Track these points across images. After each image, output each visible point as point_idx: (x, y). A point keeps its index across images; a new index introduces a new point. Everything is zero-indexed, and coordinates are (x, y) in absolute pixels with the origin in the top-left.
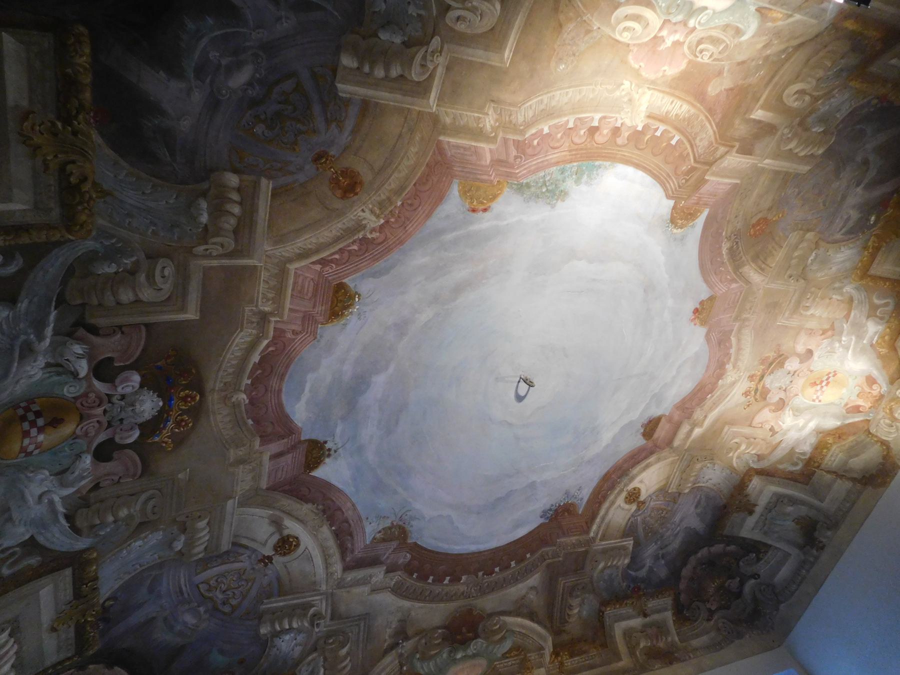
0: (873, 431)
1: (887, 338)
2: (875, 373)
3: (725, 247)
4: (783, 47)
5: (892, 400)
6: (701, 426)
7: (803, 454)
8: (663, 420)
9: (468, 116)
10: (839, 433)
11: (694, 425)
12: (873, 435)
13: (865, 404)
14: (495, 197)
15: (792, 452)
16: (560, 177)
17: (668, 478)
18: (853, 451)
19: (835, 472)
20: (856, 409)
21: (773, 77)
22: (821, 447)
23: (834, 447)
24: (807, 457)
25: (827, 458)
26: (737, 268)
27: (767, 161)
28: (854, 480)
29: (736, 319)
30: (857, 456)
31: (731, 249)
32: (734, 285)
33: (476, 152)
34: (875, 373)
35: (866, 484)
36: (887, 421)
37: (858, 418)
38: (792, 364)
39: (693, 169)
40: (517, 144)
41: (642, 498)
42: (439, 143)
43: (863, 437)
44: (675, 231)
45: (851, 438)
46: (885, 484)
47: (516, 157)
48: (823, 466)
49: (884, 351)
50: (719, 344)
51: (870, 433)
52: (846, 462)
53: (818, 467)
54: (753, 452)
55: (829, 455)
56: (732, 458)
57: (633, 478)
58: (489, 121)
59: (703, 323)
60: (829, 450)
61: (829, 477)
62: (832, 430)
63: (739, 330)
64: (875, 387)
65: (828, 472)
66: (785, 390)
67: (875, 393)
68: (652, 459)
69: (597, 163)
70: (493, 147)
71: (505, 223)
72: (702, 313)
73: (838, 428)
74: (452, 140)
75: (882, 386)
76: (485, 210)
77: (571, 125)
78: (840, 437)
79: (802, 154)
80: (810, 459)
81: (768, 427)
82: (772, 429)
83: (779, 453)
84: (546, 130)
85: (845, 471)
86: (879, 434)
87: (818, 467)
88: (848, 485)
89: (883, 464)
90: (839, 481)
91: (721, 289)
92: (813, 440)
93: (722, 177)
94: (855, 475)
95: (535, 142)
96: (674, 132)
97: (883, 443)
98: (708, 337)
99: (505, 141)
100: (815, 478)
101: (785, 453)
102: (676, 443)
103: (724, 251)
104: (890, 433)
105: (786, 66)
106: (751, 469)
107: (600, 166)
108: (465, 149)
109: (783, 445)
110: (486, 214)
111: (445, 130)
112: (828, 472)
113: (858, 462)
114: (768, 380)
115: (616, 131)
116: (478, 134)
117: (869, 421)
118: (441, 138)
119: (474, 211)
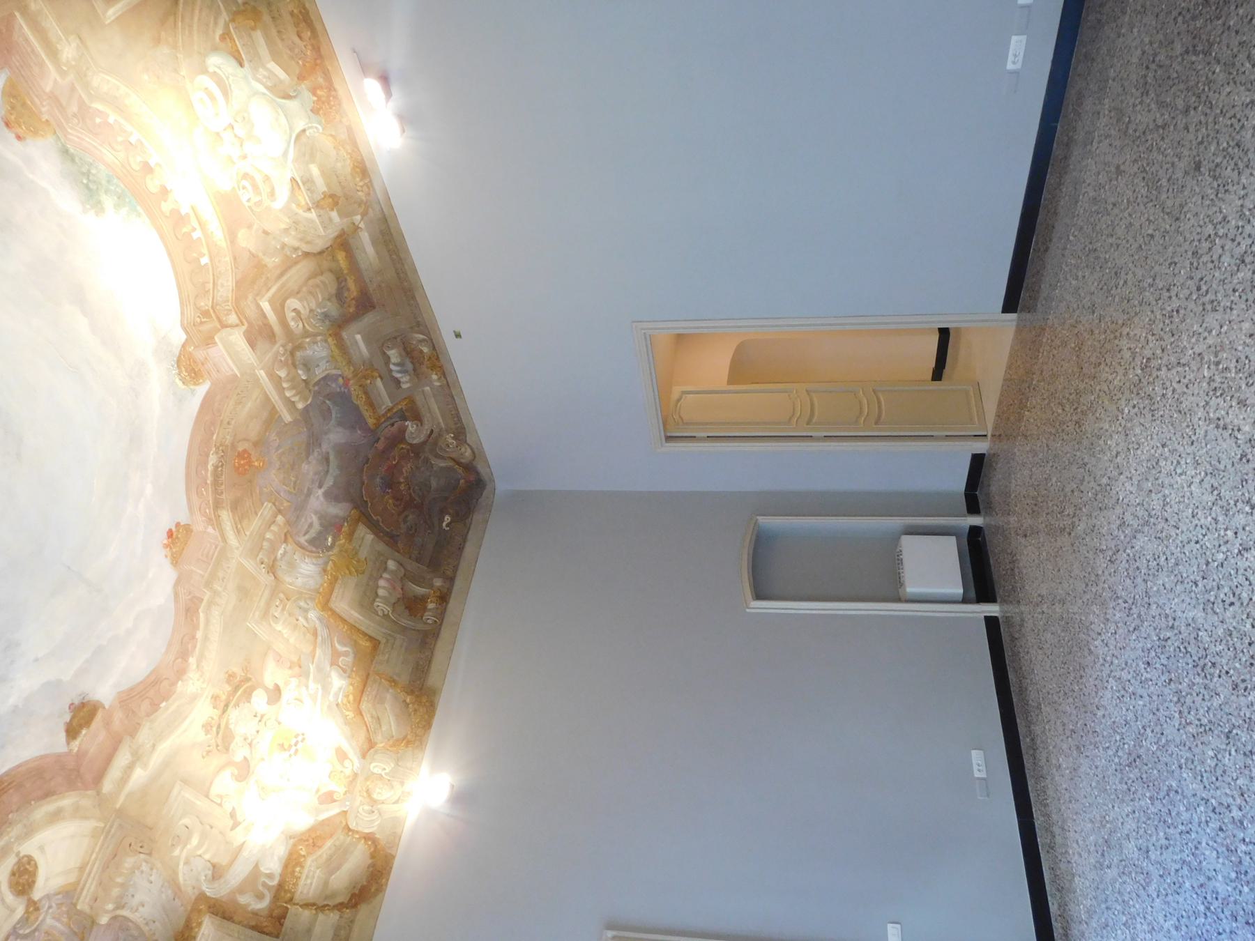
0: (353, 826)
1: (351, 698)
2: (346, 747)
3: (213, 459)
4: (296, 244)
5: (367, 779)
6: (145, 766)
7: (270, 876)
8: (99, 716)
9: (51, 24)
10: (312, 839)
11: (137, 758)
12: (353, 831)
13: (340, 789)
14: (35, 133)
15: (255, 872)
16: (104, 182)
17: (82, 869)
18: (332, 865)
19: (314, 904)
20: (329, 798)
21: (282, 274)
22: (292, 862)
23: (309, 861)
24: (275, 882)
25: (302, 882)
26: (217, 505)
27: (262, 372)
28: (340, 907)
29: (208, 584)
30: (338, 868)
31: (216, 467)
32: (210, 530)
33: (42, 65)
34: (346, 747)
35: (355, 906)
36: (367, 808)
37: (333, 810)
38: (259, 697)
39: (206, 314)
40: (82, 104)
41: (37, 895)
42: (12, 16)
43: (342, 837)
44: (177, 380)
45: (329, 843)
46: (380, 889)
47: (75, 115)
48: (297, 898)
49: (351, 714)
50: (187, 610)
51: (349, 830)
52: (326, 883)
53: (291, 899)
54: (207, 857)
55: (304, 877)
56: (178, 857)
57: (29, 832)
58: (68, 51)
59: (175, 560)
60: (302, 867)
61: (306, 914)
62: (303, 834)
63: (210, 603)
64: (347, 763)
65: (306, 905)
66: (250, 744)
67: (348, 772)
68: (67, 801)
69: (139, 208)
70: (58, 78)
71: (31, 176)
72: (177, 538)
73: (312, 829)
74: (27, 30)
75: (354, 762)
76: (19, 138)
77: (133, 140)
78: (314, 845)
79: (288, 394)
80: (280, 886)
81: (228, 807)
82: (233, 815)
83: (237, 874)
84: (111, 120)
85: (327, 898)
86: (360, 829)
87: (291, 899)
88: (334, 917)
89: (373, 865)
90: (321, 917)
91: (199, 525)
92: (281, 851)
93: (229, 354)
94: (339, 900)
95: (98, 120)
96: (205, 251)
97: (369, 838)
98: (178, 583)
99: (73, 89)
100: (288, 923)
101: (242, 876)
102: (107, 786)
103: (210, 467)
104: (373, 821)
105: (293, 271)
106: (202, 897)
107: (139, 215)
108: (33, 51)
109: (245, 854)
110: (15, 141)
111: (24, 10)
112: (306, 905)
113: (341, 879)
114: (233, 714)
115: (164, 191)
116: (53, 53)
117: (345, 812)
118: (17, 14)
119: (7, 124)
